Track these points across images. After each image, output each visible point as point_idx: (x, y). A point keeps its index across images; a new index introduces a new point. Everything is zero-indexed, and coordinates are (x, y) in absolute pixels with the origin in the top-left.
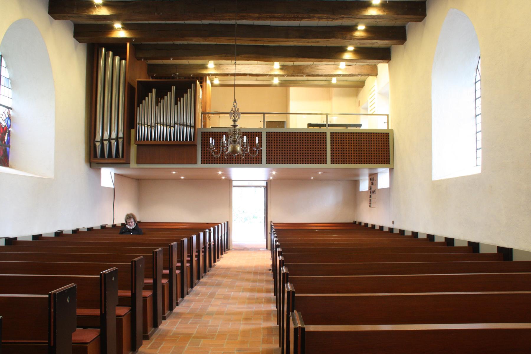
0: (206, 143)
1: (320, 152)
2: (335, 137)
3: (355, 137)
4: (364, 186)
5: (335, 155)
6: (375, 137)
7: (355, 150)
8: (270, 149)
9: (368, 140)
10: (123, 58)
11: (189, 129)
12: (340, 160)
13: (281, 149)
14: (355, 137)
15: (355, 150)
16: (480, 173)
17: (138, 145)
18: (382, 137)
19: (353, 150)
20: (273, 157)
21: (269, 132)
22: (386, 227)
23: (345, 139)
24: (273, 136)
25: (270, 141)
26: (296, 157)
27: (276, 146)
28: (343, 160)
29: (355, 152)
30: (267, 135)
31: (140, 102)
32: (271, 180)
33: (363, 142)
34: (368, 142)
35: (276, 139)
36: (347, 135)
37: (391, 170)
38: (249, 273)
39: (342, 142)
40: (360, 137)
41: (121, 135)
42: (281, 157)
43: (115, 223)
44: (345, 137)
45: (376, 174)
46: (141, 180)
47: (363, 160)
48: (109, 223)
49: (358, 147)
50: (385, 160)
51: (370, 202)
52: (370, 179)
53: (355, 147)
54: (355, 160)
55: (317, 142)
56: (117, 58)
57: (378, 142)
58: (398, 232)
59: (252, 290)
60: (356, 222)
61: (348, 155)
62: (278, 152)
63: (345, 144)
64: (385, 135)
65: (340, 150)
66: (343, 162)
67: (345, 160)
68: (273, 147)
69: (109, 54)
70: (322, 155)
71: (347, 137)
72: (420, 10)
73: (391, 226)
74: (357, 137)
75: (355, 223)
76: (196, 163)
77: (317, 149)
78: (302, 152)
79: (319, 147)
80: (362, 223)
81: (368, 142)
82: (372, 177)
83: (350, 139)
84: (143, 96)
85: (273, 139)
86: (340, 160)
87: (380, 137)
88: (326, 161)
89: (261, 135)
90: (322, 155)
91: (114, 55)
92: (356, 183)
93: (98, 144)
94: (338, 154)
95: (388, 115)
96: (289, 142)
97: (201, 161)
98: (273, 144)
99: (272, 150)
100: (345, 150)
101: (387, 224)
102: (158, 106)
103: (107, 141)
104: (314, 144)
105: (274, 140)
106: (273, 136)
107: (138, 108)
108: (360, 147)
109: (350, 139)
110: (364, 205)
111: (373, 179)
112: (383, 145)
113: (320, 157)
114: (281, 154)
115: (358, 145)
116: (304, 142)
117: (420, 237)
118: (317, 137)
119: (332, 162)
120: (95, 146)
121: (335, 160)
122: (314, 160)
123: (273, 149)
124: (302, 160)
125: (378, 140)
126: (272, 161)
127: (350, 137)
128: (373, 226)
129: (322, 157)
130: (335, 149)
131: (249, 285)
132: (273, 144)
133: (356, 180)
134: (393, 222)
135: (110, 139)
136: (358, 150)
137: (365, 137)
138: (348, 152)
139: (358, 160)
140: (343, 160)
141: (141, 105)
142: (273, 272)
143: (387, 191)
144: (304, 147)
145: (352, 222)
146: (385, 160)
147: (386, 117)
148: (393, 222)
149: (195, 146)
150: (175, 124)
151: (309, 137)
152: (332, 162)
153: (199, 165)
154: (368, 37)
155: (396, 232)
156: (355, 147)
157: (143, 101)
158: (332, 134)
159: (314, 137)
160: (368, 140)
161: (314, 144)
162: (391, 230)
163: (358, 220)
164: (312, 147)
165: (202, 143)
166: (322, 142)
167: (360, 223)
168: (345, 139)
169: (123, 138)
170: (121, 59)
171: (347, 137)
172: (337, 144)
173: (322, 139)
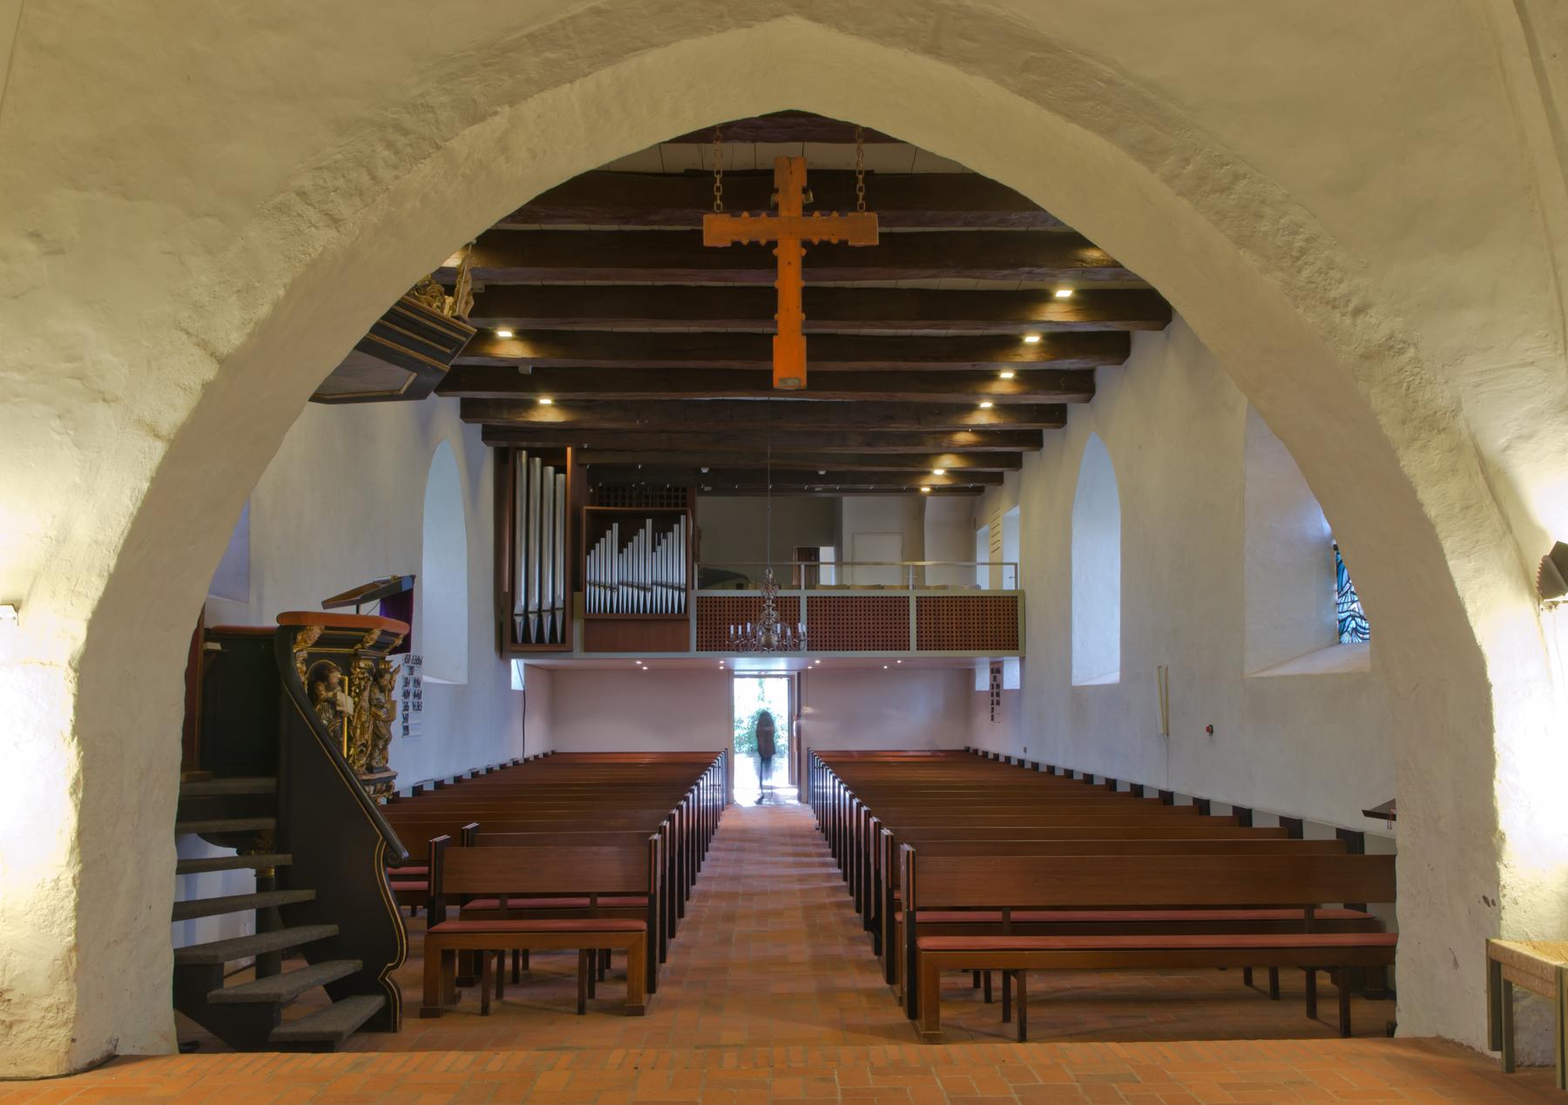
0: (704, 616)
1: (897, 630)
2: (924, 604)
3: (958, 604)
4: (983, 682)
5: (924, 634)
6: (993, 604)
7: (959, 625)
8: (814, 626)
9: (980, 608)
10: (560, 469)
11: (676, 594)
12: (933, 643)
13: (832, 626)
14: (958, 604)
15: (959, 625)
16: (1117, 684)
17: (587, 620)
18: (1006, 604)
19: (954, 625)
20: (819, 639)
21: (812, 597)
22: (1060, 768)
23: (941, 608)
24: (819, 604)
25: (815, 613)
26: (858, 639)
27: (823, 621)
28: (937, 643)
29: (959, 630)
30: (808, 602)
31: (591, 546)
32: (807, 670)
33: (971, 612)
34: (980, 613)
35: (823, 608)
36: (945, 600)
37: (1022, 660)
38: (784, 835)
39: (937, 612)
40: (967, 604)
41: (559, 604)
42: (832, 639)
43: (526, 756)
44: (941, 604)
45: (1001, 663)
46: (555, 670)
47: (972, 643)
48: (518, 756)
49: (963, 621)
50: (1011, 643)
51: (992, 712)
52: (992, 671)
53: (958, 621)
54: (959, 643)
55: (893, 612)
56: (551, 469)
57: (997, 613)
58: (1128, 789)
59: (795, 855)
60: (968, 748)
61: (946, 634)
62: (828, 630)
63: (941, 617)
64: (1010, 600)
65: (933, 625)
66: (939, 647)
67: (941, 643)
68: (819, 621)
69: (534, 462)
70: (902, 634)
71: (945, 604)
72: (1057, 414)
73: (1021, 755)
74: (962, 604)
75: (967, 749)
76: (688, 650)
77: (893, 626)
78: (867, 630)
79: (898, 621)
80: (1094, 778)
81: (980, 613)
82: (996, 666)
83: (950, 608)
84: (596, 536)
85: (819, 608)
86: (933, 643)
87: (1001, 604)
88: (909, 645)
89: (799, 602)
90: (902, 634)
91: (543, 465)
92: (968, 675)
93: (519, 620)
94: (928, 634)
95: (1016, 565)
96: (845, 613)
97: (697, 646)
98: (819, 617)
99: (817, 628)
100: (941, 625)
101: (1016, 753)
102: (622, 552)
103: (536, 615)
104: (889, 617)
105: (821, 610)
106: (819, 604)
107: (588, 557)
108: (967, 621)
109: (950, 608)
110: (983, 716)
111: (996, 671)
112: (1006, 617)
113: (898, 639)
114: (832, 635)
115: (963, 617)
116: (871, 612)
117: (1215, 812)
118: (893, 604)
119: (920, 647)
120: (513, 622)
121: (924, 643)
122: (889, 643)
123: (819, 626)
124: (867, 643)
125: (997, 608)
126: (817, 645)
127: (950, 604)
128: (997, 756)
129: (902, 639)
130: (924, 639)
131: (790, 849)
132: (819, 617)
133: (970, 670)
134: (1025, 750)
135: (540, 612)
136: (963, 625)
137: (976, 604)
138: (946, 630)
139: (963, 643)
140: (937, 643)
141: (592, 552)
142: (823, 832)
143: (1018, 694)
144: (871, 621)
145: (963, 748)
146: (1011, 643)
147: (1013, 567)
148: (1025, 750)
149: (688, 620)
150: (652, 584)
151: (880, 604)
152: (920, 647)
153: (693, 653)
154: (979, 442)
155: (1122, 788)
156: (958, 621)
157: (597, 545)
158: (919, 599)
159: (889, 604)
160: (980, 608)
161: (889, 617)
162: (1021, 762)
163: (974, 745)
164: (885, 621)
165: (698, 615)
166: (902, 612)
167: (976, 751)
168: (941, 608)
169: (564, 609)
170: (556, 472)
171: (945, 604)
172: (928, 617)
173: (902, 608)
